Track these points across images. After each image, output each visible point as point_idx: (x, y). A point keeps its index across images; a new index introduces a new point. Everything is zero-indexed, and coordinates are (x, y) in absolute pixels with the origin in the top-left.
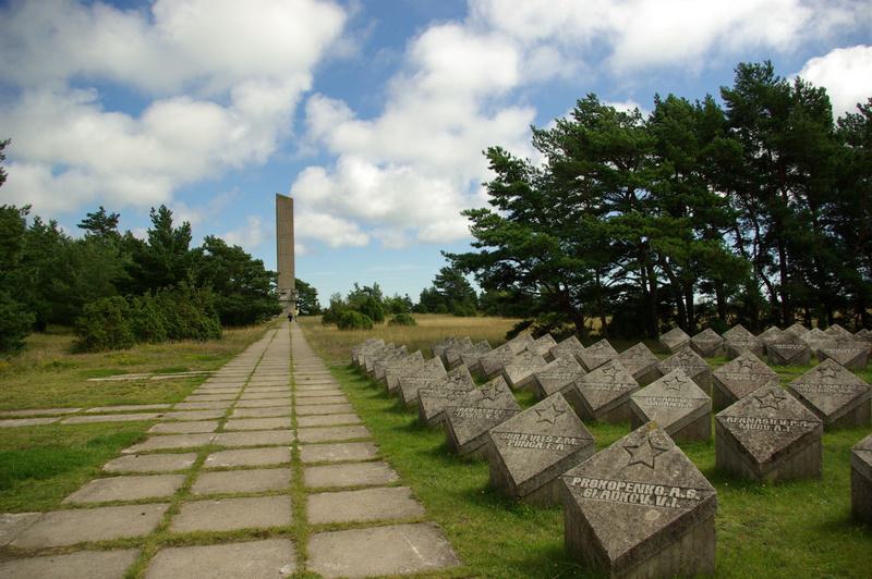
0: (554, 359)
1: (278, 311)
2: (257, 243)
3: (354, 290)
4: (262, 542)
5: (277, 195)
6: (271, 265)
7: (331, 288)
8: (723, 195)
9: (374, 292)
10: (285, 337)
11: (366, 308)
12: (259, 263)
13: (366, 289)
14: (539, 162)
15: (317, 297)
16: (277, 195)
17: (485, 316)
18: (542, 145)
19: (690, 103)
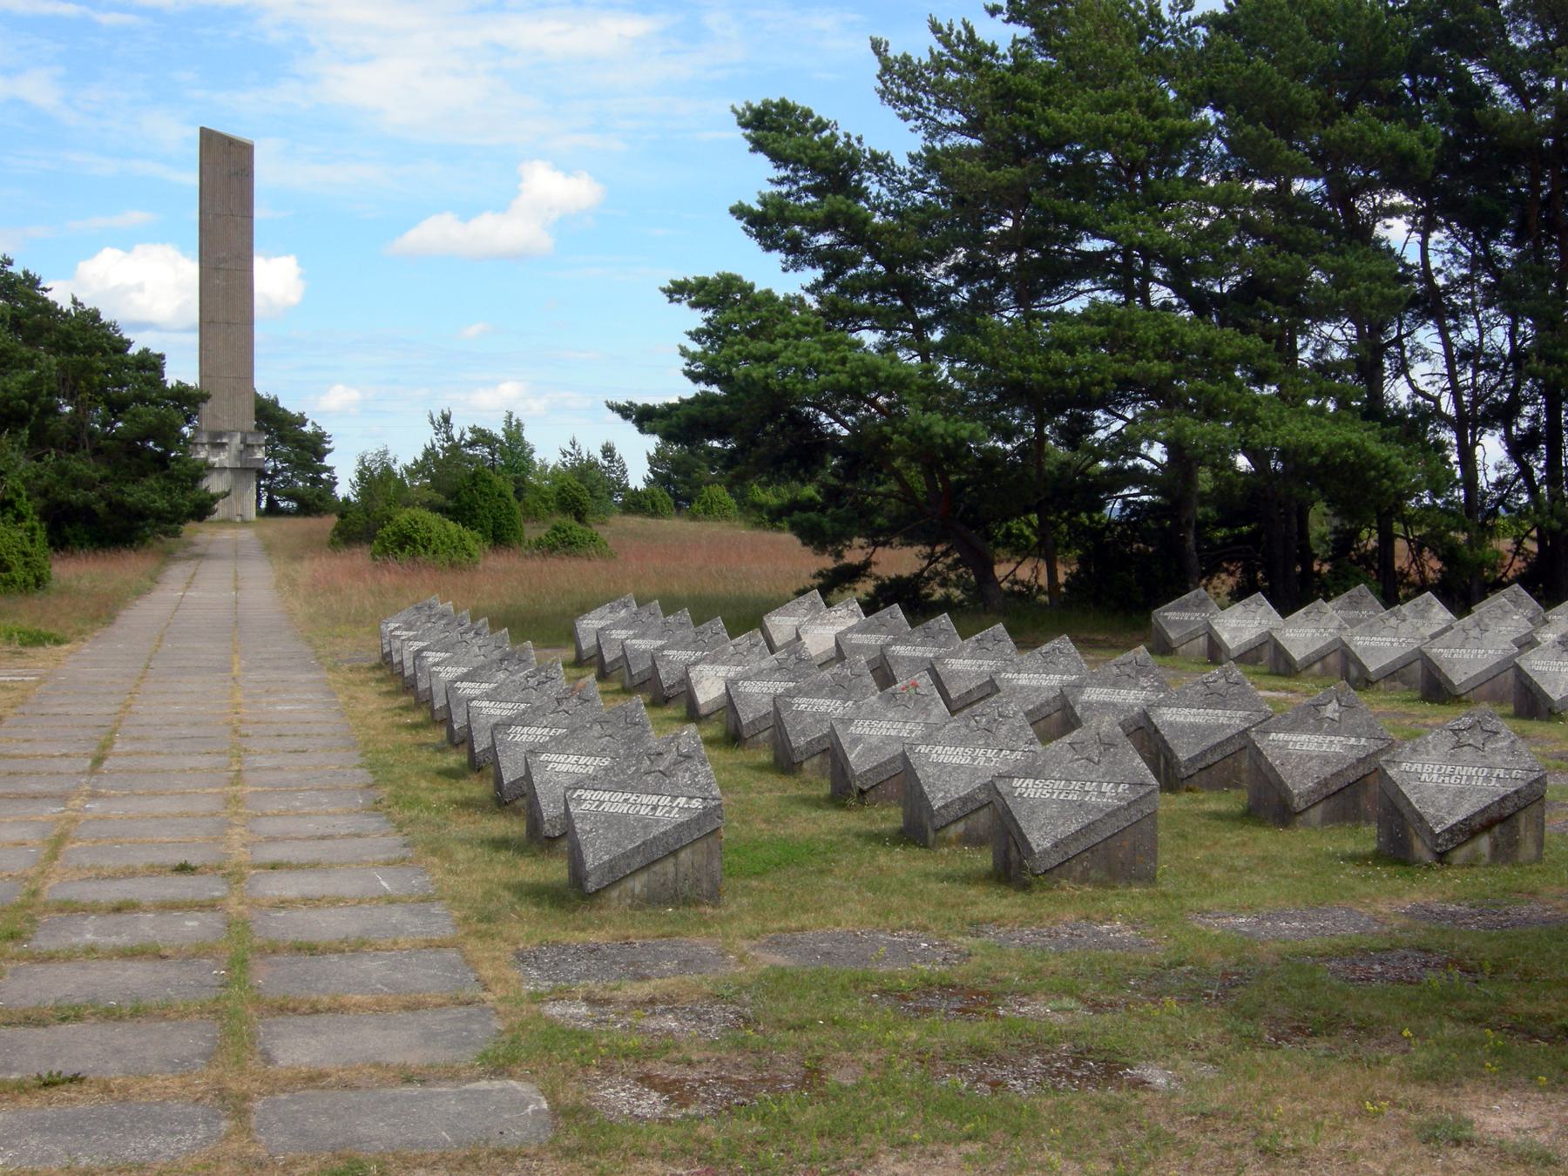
0: (1221, 664)
1: (202, 510)
2: (142, 290)
3: (439, 443)
4: (305, 937)
5: (207, 136)
6: (182, 370)
7: (371, 427)
8: (958, 365)
9: (511, 448)
10: (225, 589)
11: (477, 497)
12: (151, 364)
13: (482, 437)
14: (896, 138)
15: (328, 461)
16: (207, 136)
17: (757, 525)
18: (911, 101)
19: (689, 395)
